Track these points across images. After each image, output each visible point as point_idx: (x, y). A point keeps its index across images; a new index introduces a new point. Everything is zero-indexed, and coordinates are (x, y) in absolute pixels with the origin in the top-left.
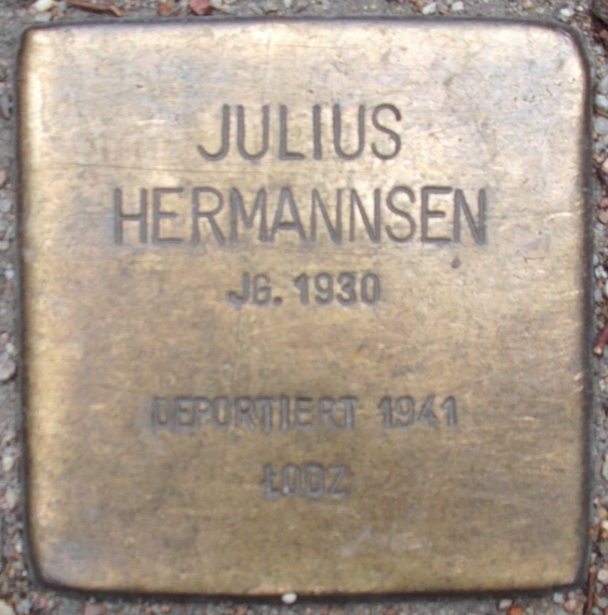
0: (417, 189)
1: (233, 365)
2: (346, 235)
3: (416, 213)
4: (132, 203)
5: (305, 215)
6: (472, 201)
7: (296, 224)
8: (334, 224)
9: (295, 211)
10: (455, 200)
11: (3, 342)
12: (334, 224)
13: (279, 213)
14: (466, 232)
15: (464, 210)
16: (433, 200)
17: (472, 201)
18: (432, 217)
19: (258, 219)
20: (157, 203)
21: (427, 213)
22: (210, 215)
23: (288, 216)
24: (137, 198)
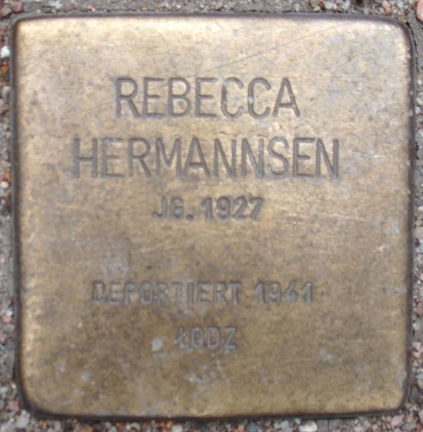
0: (290, 137)
1: (134, 284)
2: (239, 172)
3: (289, 155)
4: (85, 147)
5: (210, 160)
6: (329, 147)
7: (203, 164)
8: (230, 163)
9: (202, 156)
10: (317, 145)
11: (197, 2)
12: (230, 163)
13: (191, 154)
14: (324, 169)
15: (324, 156)
16: (152, 85)
17: (329, 147)
18: (175, 98)
19: (175, 160)
20: (105, 146)
21: (298, 156)
22: (129, 98)
23: (197, 159)
24: (90, 146)
